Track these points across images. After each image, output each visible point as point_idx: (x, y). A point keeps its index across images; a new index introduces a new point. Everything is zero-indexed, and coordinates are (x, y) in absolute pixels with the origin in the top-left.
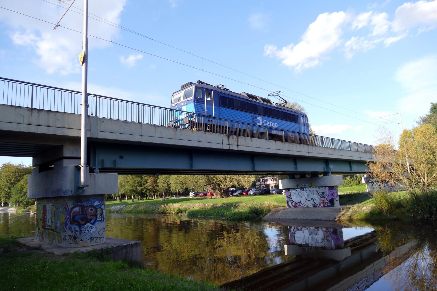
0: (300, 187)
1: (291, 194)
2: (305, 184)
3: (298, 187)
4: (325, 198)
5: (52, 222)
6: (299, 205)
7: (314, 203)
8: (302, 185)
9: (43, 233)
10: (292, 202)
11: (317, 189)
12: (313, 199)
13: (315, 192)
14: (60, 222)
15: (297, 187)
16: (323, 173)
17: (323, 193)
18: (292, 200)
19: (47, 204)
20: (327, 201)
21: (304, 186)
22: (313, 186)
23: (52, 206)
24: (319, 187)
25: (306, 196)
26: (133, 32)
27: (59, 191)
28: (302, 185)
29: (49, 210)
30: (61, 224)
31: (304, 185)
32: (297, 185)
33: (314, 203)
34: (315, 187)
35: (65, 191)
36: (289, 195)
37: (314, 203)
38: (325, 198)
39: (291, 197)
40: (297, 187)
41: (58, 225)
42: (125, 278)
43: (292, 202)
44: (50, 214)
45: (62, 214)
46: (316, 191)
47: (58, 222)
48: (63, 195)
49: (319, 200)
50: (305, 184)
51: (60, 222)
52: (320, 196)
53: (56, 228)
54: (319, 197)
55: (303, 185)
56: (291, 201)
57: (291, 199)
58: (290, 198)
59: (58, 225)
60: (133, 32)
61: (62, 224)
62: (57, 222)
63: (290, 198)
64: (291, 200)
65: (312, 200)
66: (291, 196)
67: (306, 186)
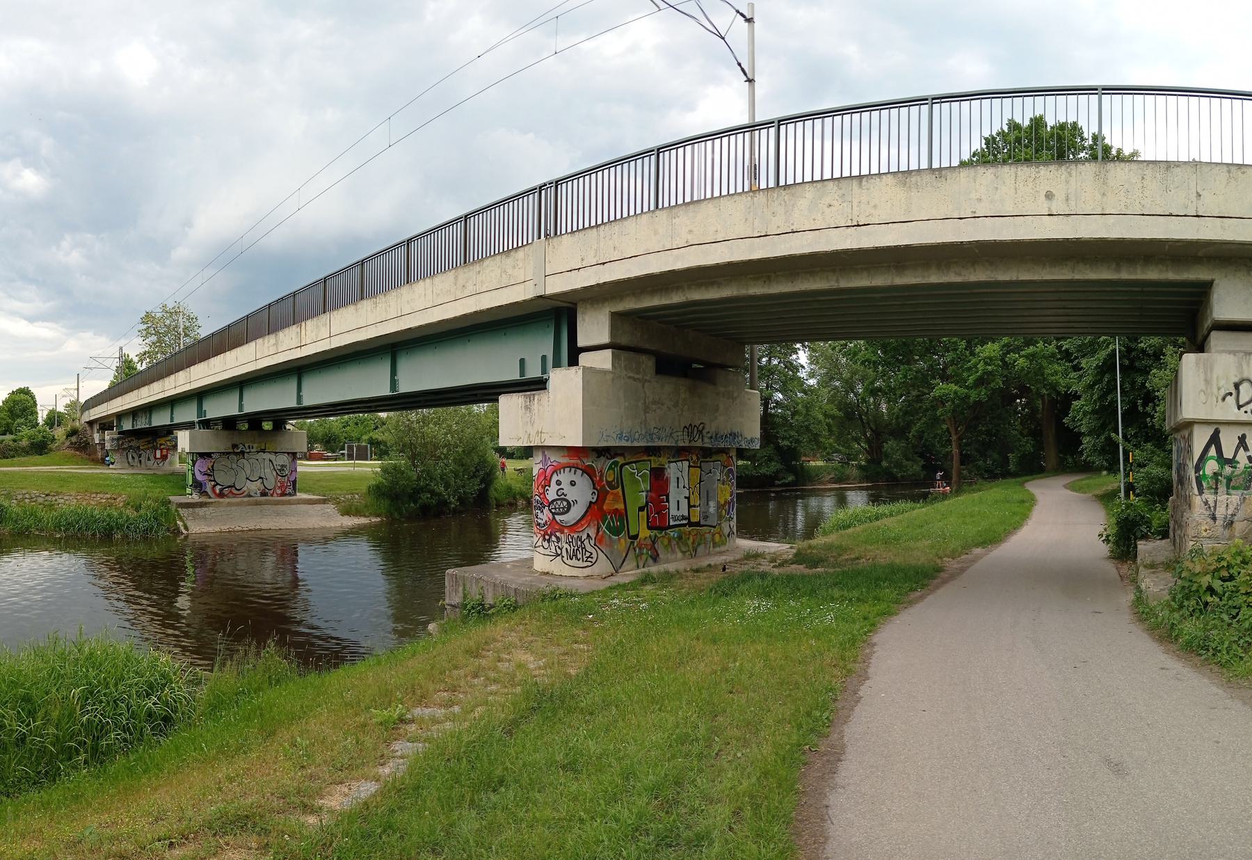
0: (239, 451)
1: (212, 467)
2: (251, 444)
3: (236, 450)
4: (285, 476)
5: (690, 506)
6: (231, 491)
7: (262, 488)
8: (244, 446)
9: (654, 542)
10: (214, 486)
11: (272, 457)
12: (262, 478)
13: (267, 462)
14: (718, 502)
15: (233, 449)
16: (223, 422)
17: (282, 466)
18: (214, 481)
19: (670, 462)
20: (289, 484)
21: (249, 448)
22: (269, 449)
23: (689, 466)
24: (276, 453)
25: (248, 472)
26: (507, 39)
27: (734, 435)
28: (244, 446)
29: (678, 478)
30: (720, 507)
31: (249, 446)
32: (232, 446)
33: (262, 488)
34: (269, 452)
35: (749, 439)
36: (209, 469)
37: (264, 488)
38: (285, 476)
39: (212, 474)
40: (232, 451)
41: (712, 510)
42: (735, 588)
43: (214, 486)
44: (684, 487)
45: (723, 484)
46: (270, 460)
47: (712, 504)
48: (744, 445)
49: (273, 480)
50: (251, 444)
51: (718, 502)
52: (277, 473)
53: (706, 517)
54: (275, 473)
55: (247, 445)
56: (213, 483)
57: (212, 479)
58: (211, 476)
59: (712, 510)
60: (507, 39)
61: (724, 506)
62: (708, 504)
63: (211, 476)
64: (211, 481)
65: (260, 481)
66: (213, 470)
67: (252, 448)
